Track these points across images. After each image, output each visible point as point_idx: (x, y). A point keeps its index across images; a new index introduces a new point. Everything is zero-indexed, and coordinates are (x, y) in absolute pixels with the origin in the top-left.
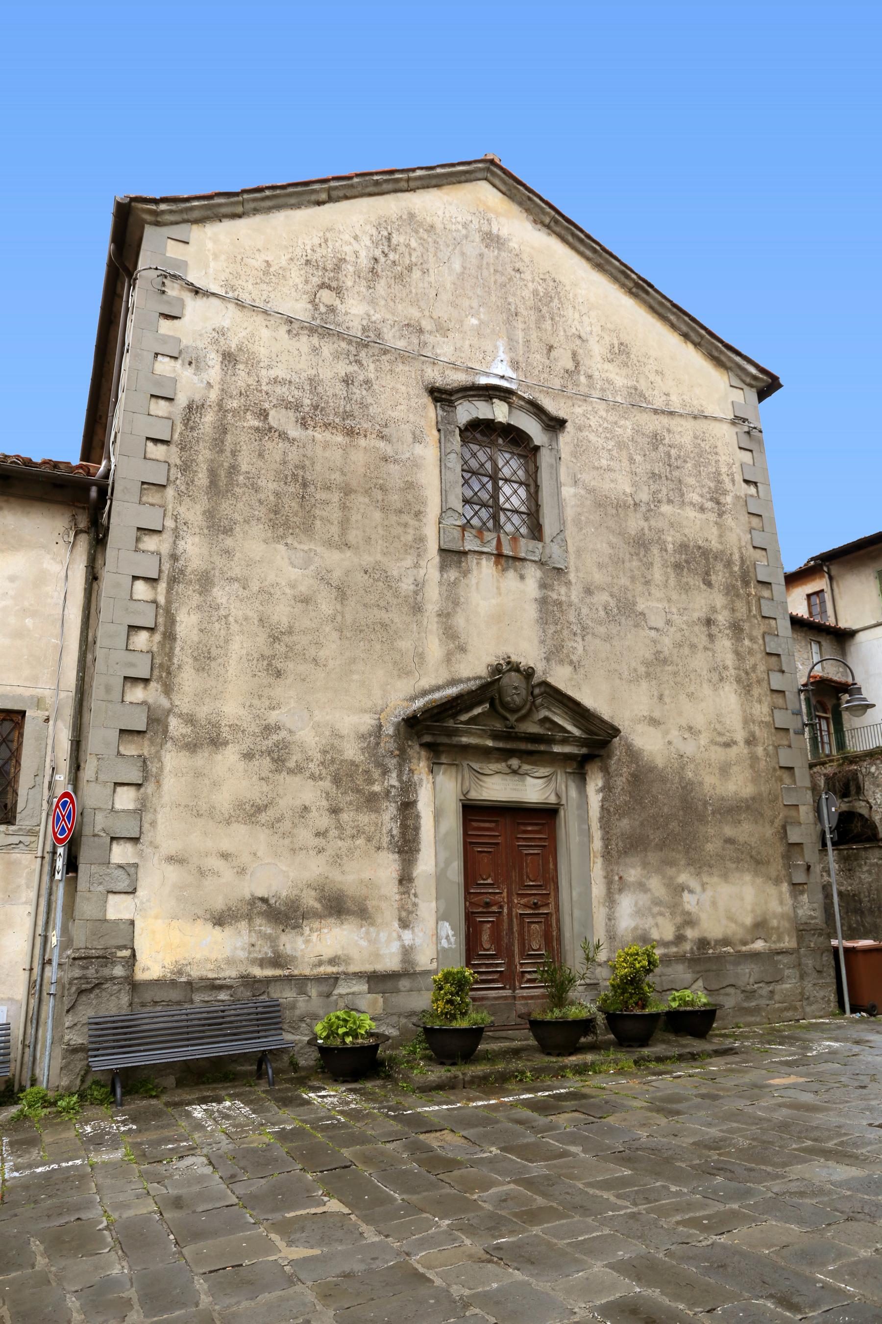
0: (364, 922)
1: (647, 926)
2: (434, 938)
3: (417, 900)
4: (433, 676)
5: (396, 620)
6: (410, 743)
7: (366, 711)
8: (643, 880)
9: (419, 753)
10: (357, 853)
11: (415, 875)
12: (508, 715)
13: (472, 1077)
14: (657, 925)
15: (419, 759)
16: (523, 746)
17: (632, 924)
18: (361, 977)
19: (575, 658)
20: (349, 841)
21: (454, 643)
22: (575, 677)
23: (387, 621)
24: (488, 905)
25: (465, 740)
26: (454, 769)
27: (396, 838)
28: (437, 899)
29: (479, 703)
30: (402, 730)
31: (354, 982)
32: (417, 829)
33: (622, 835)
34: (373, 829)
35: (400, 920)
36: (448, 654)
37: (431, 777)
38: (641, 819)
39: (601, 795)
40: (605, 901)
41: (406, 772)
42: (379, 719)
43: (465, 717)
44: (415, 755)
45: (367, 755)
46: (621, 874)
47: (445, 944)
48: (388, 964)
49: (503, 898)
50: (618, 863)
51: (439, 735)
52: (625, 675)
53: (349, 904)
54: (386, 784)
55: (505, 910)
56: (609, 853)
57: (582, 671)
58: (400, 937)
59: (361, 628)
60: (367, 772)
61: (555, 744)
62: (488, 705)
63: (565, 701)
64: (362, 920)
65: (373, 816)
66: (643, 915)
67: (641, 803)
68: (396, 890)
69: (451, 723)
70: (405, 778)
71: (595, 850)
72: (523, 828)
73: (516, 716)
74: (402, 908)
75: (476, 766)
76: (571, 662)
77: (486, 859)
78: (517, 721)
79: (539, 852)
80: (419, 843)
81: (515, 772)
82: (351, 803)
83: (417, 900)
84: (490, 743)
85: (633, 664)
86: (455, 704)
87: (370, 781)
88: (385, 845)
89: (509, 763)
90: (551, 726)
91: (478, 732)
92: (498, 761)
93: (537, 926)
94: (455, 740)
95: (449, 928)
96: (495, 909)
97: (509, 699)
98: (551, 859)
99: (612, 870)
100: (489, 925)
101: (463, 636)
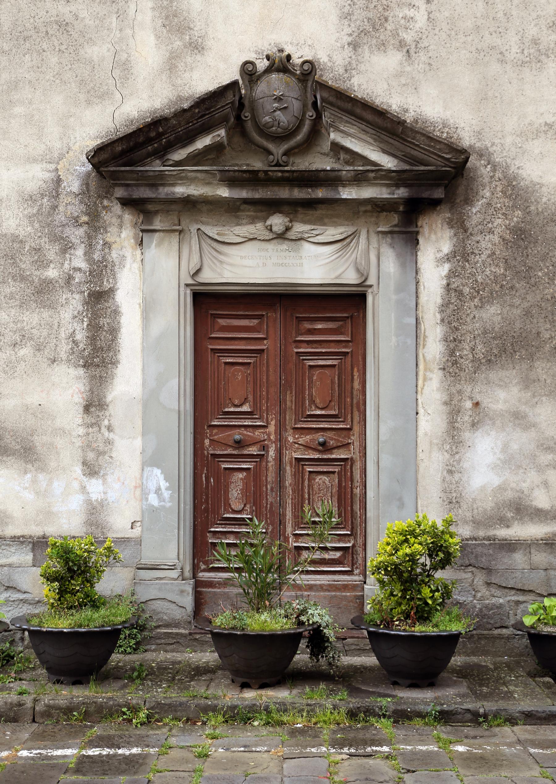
0: (29, 466)
1: (525, 486)
2: (138, 492)
3: (111, 436)
4: (145, 96)
5: (83, 14)
6: (106, 202)
7: (35, 161)
8: (523, 408)
9: (120, 217)
10: (22, 366)
11: (109, 398)
12: (271, 146)
13: (48, 706)
14: (546, 484)
15: (121, 226)
16: (284, 193)
17: (496, 481)
18: (22, 543)
19: (408, 37)
20: (9, 351)
21: (181, 39)
22: (408, 69)
23: (69, 18)
24: (239, 444)
25: (180, 190)
26: (175, 238)
27: (81, 346)
28: (144, 434)
29: (205, 130)
30: (93, 185)
31: (13, 549)
32: (114, 331)
33: (485, 332)
34: (45, 333)
35: (84, 463)
36: (170, 59)
37: (139, 252)
38: (526, 305)
39: (447, 267)
40: (444, 441)
41: (99, 247)
42: (57, 170)
43: (180, 155)
44: (114, 220)
45: (37, 225)
46: (478, 398)
47: (153, 500)
48: (66, 527)
49: (269, 435)
50: (472, 380)
51: (137, 185)
52: (514, 53)
53: (8, 440)
54: (66, 266)
55: (272, 453)
56: (455, 363)
57: (423, 57)
58: (83, 489)
59: (25, 33)
60: (38, 250)
61: (344, 186)
62: (222, 132)
63: (358, 111)
64: (26, 462)
65: (46, 314)
66: (519, 467)
67: (527, 278)
68: (80, 421)
69: (157, 167)
70: (97, 256)
71: (429, 357)
72: (307, 325)
73: (285, 147)
74: (88, 446)
75: (212, 231)
76: (402, 44)
77: (239, 374)
78: (286, 154)
79: (335, 362)
80: (117, 352)
81: (282, 236)
82: (12, 297)
83: (111, 436)
84: (224, 192)
85: (532, 31)
86: (153, 134)
87: (42, 264)
88: (63, 355)
89: (268, 222)
90: (348, 157)
91: (199, 175)
92: (253, 220)
93: (325, 478)
94: (164, 192)
95: (161, 477)
96: (253, 450)
97: (267, 119)
98: (356, 374)
99: (459, 392)
100: (241, 475)
101: (198, 26)
